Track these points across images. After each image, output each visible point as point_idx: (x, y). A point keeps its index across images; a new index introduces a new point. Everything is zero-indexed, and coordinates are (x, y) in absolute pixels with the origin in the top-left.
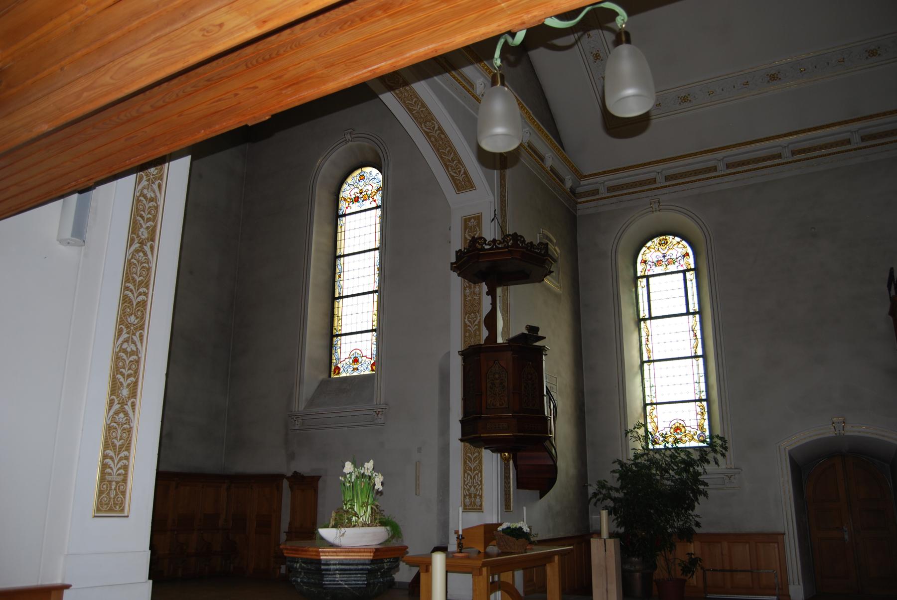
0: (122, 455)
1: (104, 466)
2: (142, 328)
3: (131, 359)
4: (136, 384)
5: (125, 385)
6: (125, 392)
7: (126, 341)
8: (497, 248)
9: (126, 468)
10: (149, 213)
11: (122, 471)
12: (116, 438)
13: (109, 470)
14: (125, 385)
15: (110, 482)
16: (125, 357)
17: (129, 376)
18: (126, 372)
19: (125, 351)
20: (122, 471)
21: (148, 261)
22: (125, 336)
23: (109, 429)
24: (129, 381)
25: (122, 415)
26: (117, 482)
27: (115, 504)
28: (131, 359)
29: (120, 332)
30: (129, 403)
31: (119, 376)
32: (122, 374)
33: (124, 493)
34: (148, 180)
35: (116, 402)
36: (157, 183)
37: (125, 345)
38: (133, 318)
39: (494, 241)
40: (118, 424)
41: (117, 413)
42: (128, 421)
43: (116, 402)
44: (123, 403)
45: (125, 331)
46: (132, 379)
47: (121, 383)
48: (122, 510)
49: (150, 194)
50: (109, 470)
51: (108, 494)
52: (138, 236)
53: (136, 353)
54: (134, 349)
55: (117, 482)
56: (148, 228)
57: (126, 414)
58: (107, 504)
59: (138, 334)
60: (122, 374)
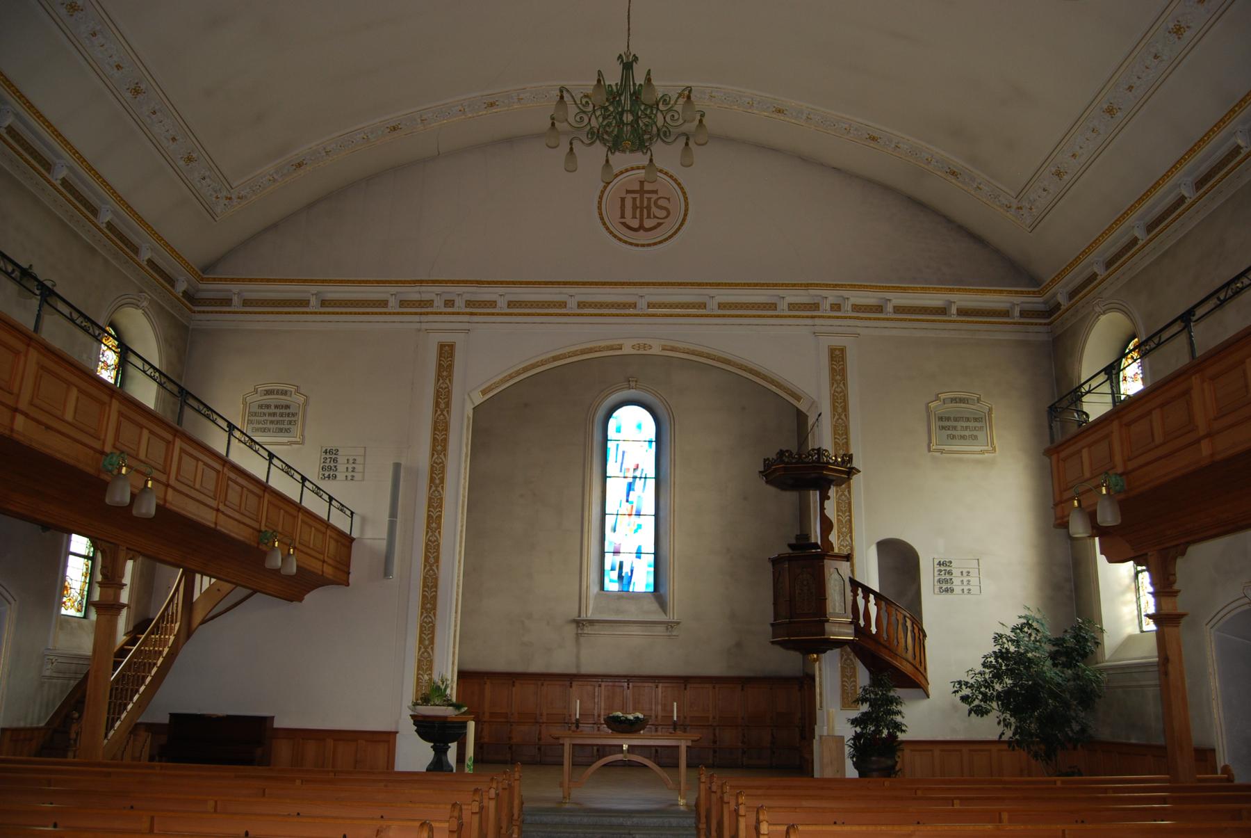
1: (843, 686)
4: (433, 638)
44: (426, 648)
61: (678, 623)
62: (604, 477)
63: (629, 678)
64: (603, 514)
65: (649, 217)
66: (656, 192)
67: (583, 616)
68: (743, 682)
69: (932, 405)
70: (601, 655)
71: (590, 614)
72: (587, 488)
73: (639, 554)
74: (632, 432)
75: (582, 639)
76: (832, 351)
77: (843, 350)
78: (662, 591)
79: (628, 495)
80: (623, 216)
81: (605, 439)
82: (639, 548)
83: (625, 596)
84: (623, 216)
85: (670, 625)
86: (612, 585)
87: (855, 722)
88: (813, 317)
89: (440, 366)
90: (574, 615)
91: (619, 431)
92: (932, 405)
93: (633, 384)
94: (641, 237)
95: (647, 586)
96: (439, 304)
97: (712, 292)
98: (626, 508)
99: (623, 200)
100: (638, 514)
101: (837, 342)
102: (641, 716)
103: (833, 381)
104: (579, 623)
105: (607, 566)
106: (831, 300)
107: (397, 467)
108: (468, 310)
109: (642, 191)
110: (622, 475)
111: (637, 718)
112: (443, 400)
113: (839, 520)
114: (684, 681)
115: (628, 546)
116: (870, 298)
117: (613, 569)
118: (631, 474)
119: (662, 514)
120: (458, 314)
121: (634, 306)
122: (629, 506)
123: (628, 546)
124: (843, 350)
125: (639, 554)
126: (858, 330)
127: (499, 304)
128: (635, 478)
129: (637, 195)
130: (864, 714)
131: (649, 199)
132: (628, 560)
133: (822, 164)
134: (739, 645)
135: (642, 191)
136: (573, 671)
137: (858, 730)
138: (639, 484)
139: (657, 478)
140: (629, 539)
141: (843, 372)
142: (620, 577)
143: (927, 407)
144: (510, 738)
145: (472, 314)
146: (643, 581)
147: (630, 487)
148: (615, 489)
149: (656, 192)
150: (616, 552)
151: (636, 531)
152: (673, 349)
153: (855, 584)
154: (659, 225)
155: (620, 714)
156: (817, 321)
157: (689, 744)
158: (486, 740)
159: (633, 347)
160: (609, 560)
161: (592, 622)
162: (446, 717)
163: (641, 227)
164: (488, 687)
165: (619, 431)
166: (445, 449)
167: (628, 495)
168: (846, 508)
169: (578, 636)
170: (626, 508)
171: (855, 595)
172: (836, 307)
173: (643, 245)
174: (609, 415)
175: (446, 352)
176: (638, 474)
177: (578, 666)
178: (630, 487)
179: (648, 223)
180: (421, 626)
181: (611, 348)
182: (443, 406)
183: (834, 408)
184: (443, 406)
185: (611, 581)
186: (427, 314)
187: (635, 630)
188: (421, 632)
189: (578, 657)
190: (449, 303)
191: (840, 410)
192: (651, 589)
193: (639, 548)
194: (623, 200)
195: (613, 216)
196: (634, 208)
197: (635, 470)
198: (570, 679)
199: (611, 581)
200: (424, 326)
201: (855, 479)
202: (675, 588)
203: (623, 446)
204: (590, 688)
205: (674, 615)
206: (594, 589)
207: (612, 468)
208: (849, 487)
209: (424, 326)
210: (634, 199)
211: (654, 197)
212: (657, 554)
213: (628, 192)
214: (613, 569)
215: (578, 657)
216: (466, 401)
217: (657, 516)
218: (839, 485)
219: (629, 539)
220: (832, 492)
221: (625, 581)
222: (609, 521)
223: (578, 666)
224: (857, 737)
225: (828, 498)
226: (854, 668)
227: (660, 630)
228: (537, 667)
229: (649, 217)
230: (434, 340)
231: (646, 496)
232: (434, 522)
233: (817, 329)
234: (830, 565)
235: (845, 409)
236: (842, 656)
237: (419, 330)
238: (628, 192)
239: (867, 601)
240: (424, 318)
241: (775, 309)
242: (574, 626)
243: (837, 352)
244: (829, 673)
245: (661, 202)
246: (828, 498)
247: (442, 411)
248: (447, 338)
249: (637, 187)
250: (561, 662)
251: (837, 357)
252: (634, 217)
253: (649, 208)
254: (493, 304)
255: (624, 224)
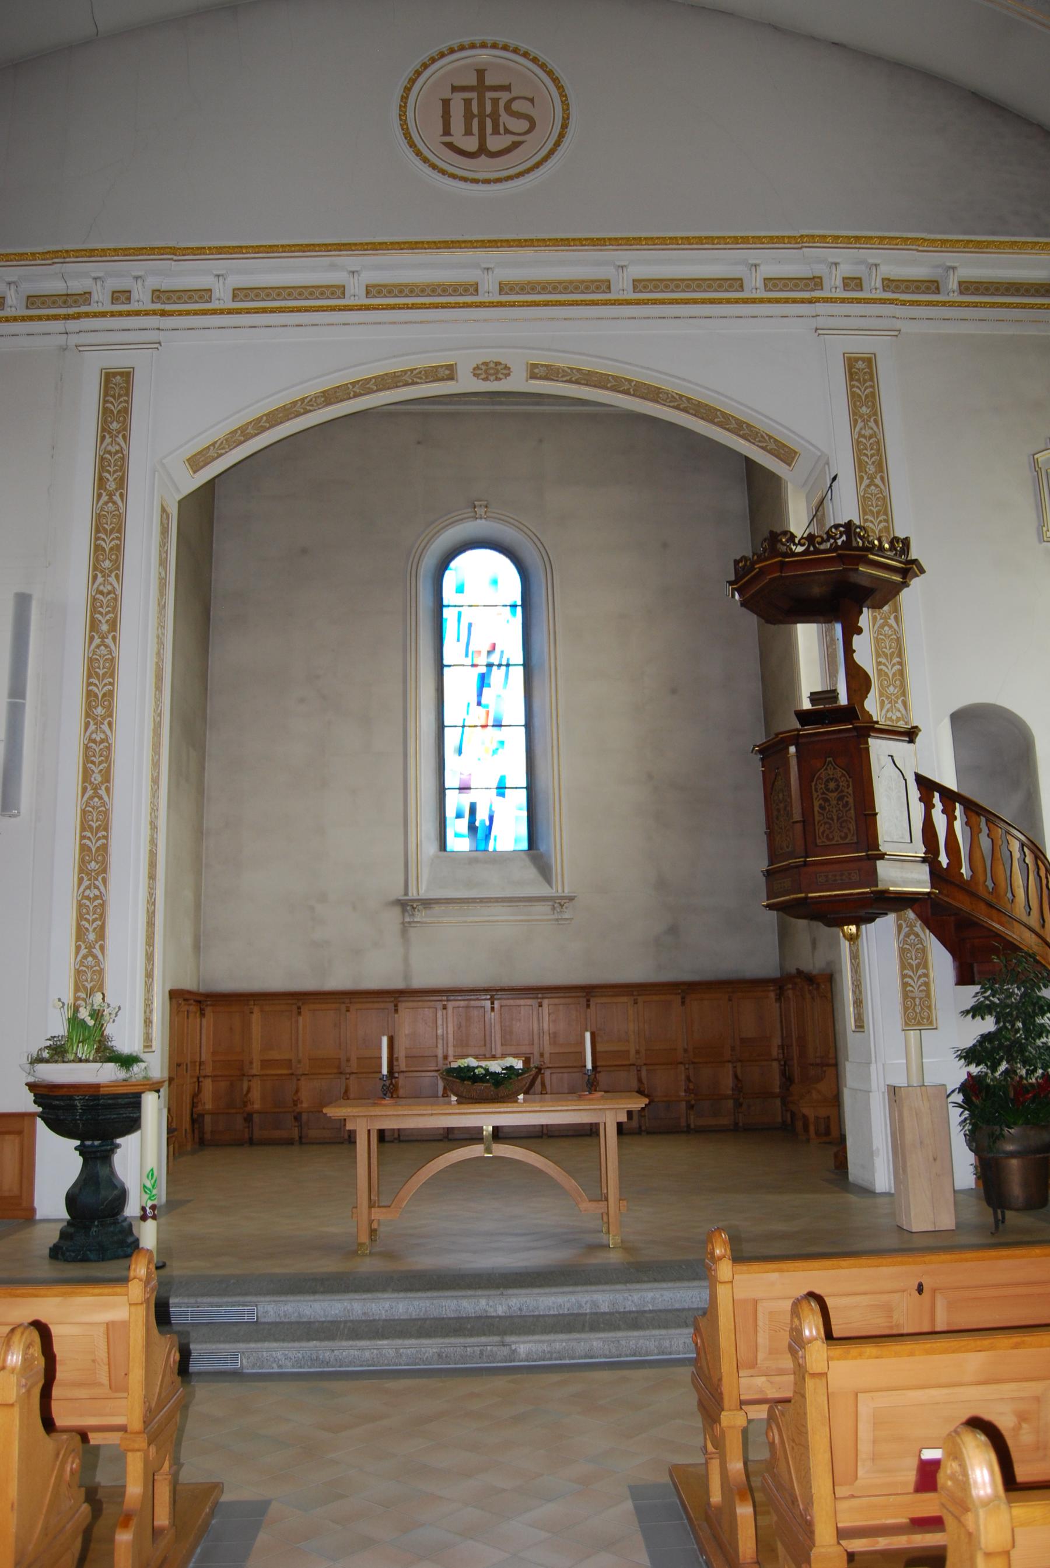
0: (920, 972)
1: (905, 985)
2: (105, 871)
3: (96, 903)
4: (102, 927)
5: (91, 929)
6: (92, 936)
7: (88, 887)
8: (817, 551)
9: (927, 984)
10: (101, 756)
11: (923, 988)
12: (87, 981)
13: (909, 988)
14: (91, 929)
15: (914, 998)
16: (88, 903)
17: (94, 920)
18: (90, 918)
19: (88, 898)
20: (923, 988)
21: (104, 804)
22: (86, 883)
23: (78, 973)
24: (95, 925)
25: (90, 959)
26: (921, 999)
27: (922, 1018)
28: (96, 903)
29: (81, 881)
30: (97, 946)
31: (84, 923)
32: (87, 920)
33: (929, 1007)
34: (890, 702)
35: (83, 947)
36: (106, 722)
37: (87, 892)
38: (93, 864)
39: (811, 538)
40: (87, 967)
41: (907, 936)
42: (98, 963)
43: (83, 947)
44: (90, 947)
45: (86, 879)
46: (99, 923)
47: (87, 929)
48: (931, 1023)
49: (98, 737)
50: (909, 988)
51: (914, 1009)
52: (91, 783)
53: (100, 897)
54: (97, 893)
55: (921, 999)
56: (101, 771)
57: (95, 957)
58: (915, 1019)
59: (100, 879)
60: (87, 920)
61: (571, 899)
62: (440, 667)
63: (493, 992)
64: (441, 727)
65: (496, 131)
66: (507, 88)
67: (413, 894)
68: (685, 990)
69: (1041, 457)
70: (439, 957)
71: (423, 889)
72: (411, 685)
73: (501, 789)
74: (482, 591)
75: (412, 932)
76: (850, 362)
77: (870, 361)
78: (542, 848)
79: (480, 694)
80: (447, 132)
81: (439, 605)
82: (502, 779)
83: (482, 857)
84: (447, 132)
85: (559, 903)
86: (459, 842)
87: (970, 1056)
88: (810, 301)
89: (106, 414)
90: (398, 893)
91: (460, 590)
92: (1041, 457)
93: (480, 511)
94: (483, 167)
95: (516, 841)
96: (101, 300)
97: (623, 256)
98: (478, 716)
99: (446, 103)
100: (498, 725)
101: (860, 345)
102: (518, 1064)
103: (855, 416)
104: (406, 905)
105: (450, 812)
106: (847, 269)
107: (23, 601)
108: (158, 306)
109: (481, 87)
110: (468, 661)
111: (510, 1069)
112: (111, 475)
113: (880, 672)
114: (586, 993)
115: (484, 778)
116: (913, 266)
117: (459, 815)
118: (483, 660)
119: (537, 722)
120: (137, 313)
121: (475, 289)
122: (481, 711)
123: (484, 778)
124: (870, 361)
125: (501, 789)
126: (898, 324)
127: (216, 294)
128: (490, 665)
129: (474, 95)
130: (985, 1038)
131: (495, 102)
132: (485, 800)
133: (813, 38)
134: (673, 930)
135: (481, 87)
136: (399, 984)
137: (974, 1069)
138: (497, 675)
139: (527, 665)
140: (485, 763)
141: (872, 399)
142: (472, 828)
143: (1036, 462)
144: (295, 1103)
145: (163, 313)
146: (510, 834)
147: (483, 681)
148: (459, 684)
149: (507, 88)
150: (464, 788)
151: (495, 752)
152: (551, 373)
153: (926, 786)
154: (516, 145)
155: (472, 1062)
156: (820, 308)
157: (623, 1118)
158: (257, 1106)
159: (476, 372)
160: (454, 801)
161: (427, 903)
162: (97, 1086)
163: (483, 150)
164: (256, 1018)
165: (460, 590)
166: (118, 565)
167: (480, 694)
168: (894, 650)
169: (405, 928)
170: (478, 716)
171: (929, 807)
172: (853, 283)
173: (487, 181)
174: (443, 565)
175: (117, 387)
176: (495, 659)
177: (407, 976)
178: (483, 681)
179: (494, 143)
180: (80, 905)
181: (433, 375)
182: (112, 485)
183: (860, 466)
184: (112, 485)
185: (457, 835)
186: (78, 316)
187: (500, 913)
188: (80, 917)
189: (406, 959)
190: (121, 296)
191: (871, 469)
192: (524, 845)
193: (502, 779)
194: (446, 103)
195: (430, 135)
196: (468, 116)
197: (489, 653)
198: (393, 998)
199: (457, 835)
200: (73, 340)
201: (911, 596)
202: (563, 842)
203: (468, 615)
204: (428, 1013)
205: (565, 883)
206: (430, 848)
207: (452, 652)
208: (896, 610)
209: (73, 340)
210: (468, 102)
211: (505, 96)
212: (530, 788)
213: (455, 89)
214: (459, 815)
215: (406, 959)
216: (161, 477)
217: (529, 726)
218: (878, 606)
219: (485, 763)
220: (866, 618)
221: (480, 834)
222: (451, 738)
223: (407, 976)
224: (971, 1088)
225: (860, 631)
226: (924, 950)
227: (542, 910)
228: (338, 980)
229: (496, 131)
230: (92, 367)
231: (508, 695)
232: (99, 704)
233: (821, 322)
234: (879, 748)
235: (881, 466)
236: (900, 928)
237: (64, 349)
238: (455, 89)
239: (951, 819)
240: (72, 325)
241: (741, 288)
242: (397, 910)
243: (860, 365)
244: (877, 958)
245: (516, 106)
246: (860, 631)
247: (111, 495)
248: (118, 360)
249: (473, 82)
250: (378, 971)
251: (860, 373)
252: (468, 132)
253: (495, 117)
254: (205, 294)
255: (450, 146)
